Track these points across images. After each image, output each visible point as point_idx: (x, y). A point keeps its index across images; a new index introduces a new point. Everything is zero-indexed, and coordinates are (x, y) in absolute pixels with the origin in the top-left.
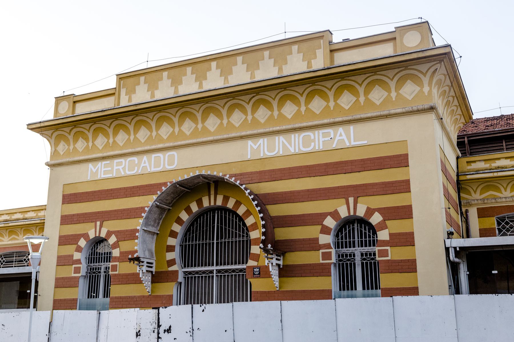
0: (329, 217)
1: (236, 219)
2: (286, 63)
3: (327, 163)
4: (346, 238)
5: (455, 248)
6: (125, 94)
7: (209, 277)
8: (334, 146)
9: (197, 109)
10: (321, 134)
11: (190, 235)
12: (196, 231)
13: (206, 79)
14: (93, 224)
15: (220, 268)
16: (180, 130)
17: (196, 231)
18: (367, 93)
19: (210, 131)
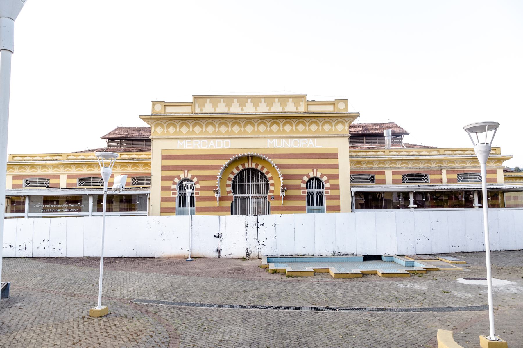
0: (325, 176)
1: (260, 174)
2: (286, 106)
3: (304, 154)
4: (311, 185)
5: (354, 191)
6: (198, 106)
7: (248, 199)
8: (308, 146)
9: (243, 121)
10: (302, 141)
11: (237, 179)
12: (240, 178)
13: (245, 106)
14: (183, 171)
15: (253, 195)
16: (232, 130)
17: (240, 178)
18: (323, 125)
19: (248, 132)
